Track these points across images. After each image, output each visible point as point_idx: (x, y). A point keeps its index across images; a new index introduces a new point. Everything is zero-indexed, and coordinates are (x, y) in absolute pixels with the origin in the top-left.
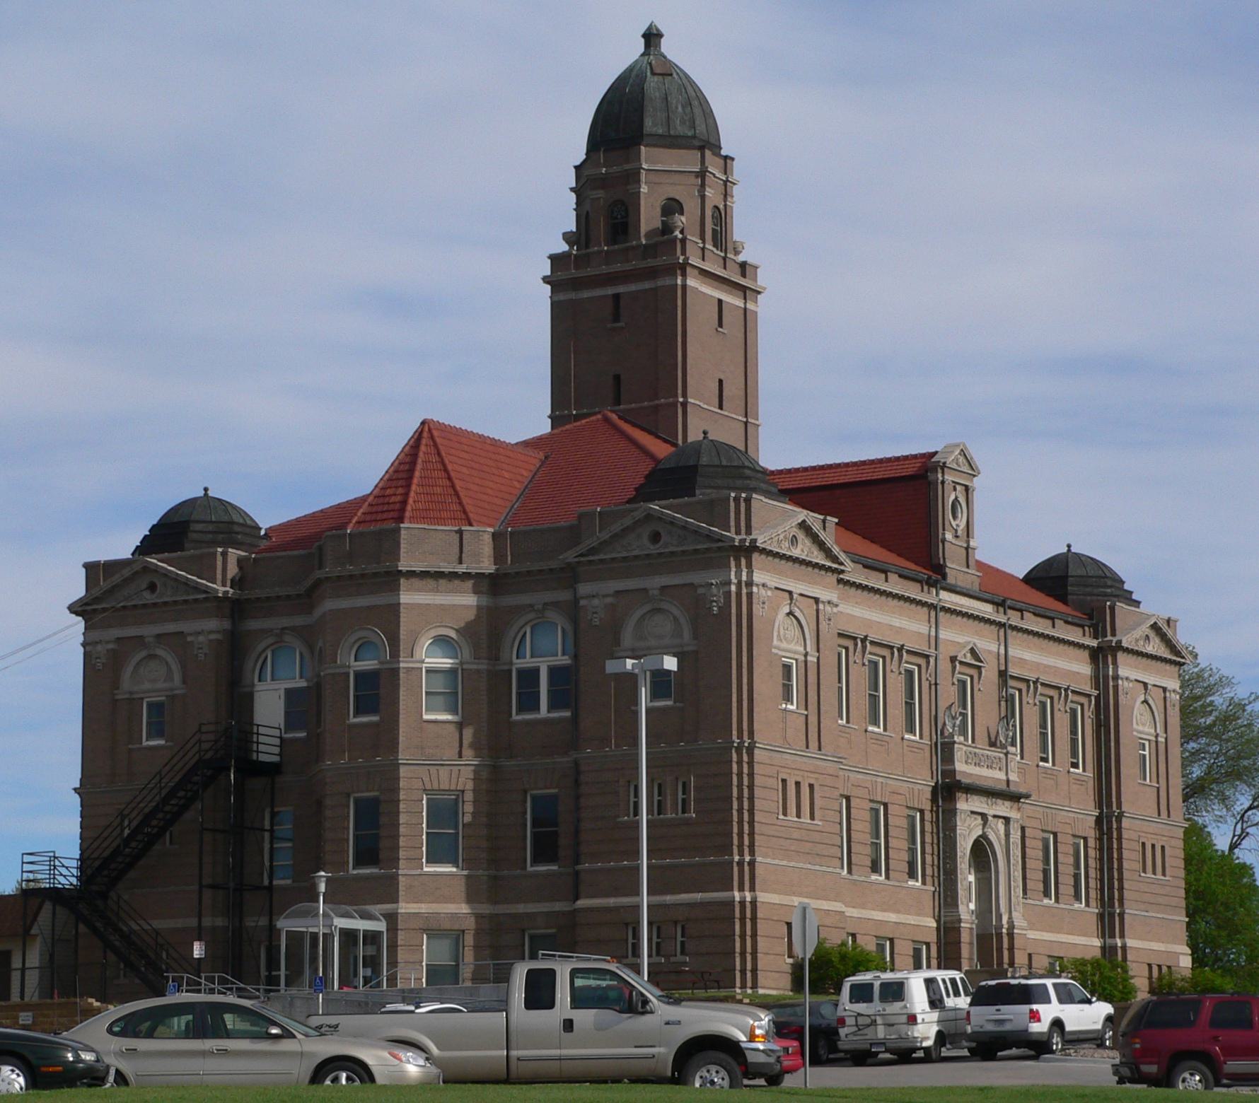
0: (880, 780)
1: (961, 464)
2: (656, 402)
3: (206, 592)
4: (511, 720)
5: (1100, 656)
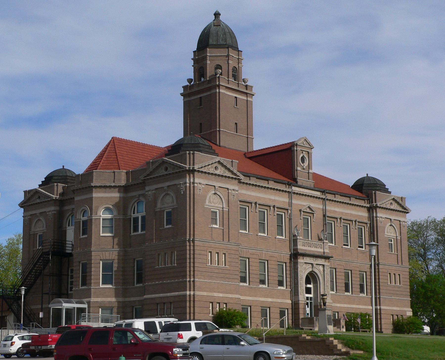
0: (264, 252)
1: (305, 144)
2: (211, 131)
4: (131, 235)
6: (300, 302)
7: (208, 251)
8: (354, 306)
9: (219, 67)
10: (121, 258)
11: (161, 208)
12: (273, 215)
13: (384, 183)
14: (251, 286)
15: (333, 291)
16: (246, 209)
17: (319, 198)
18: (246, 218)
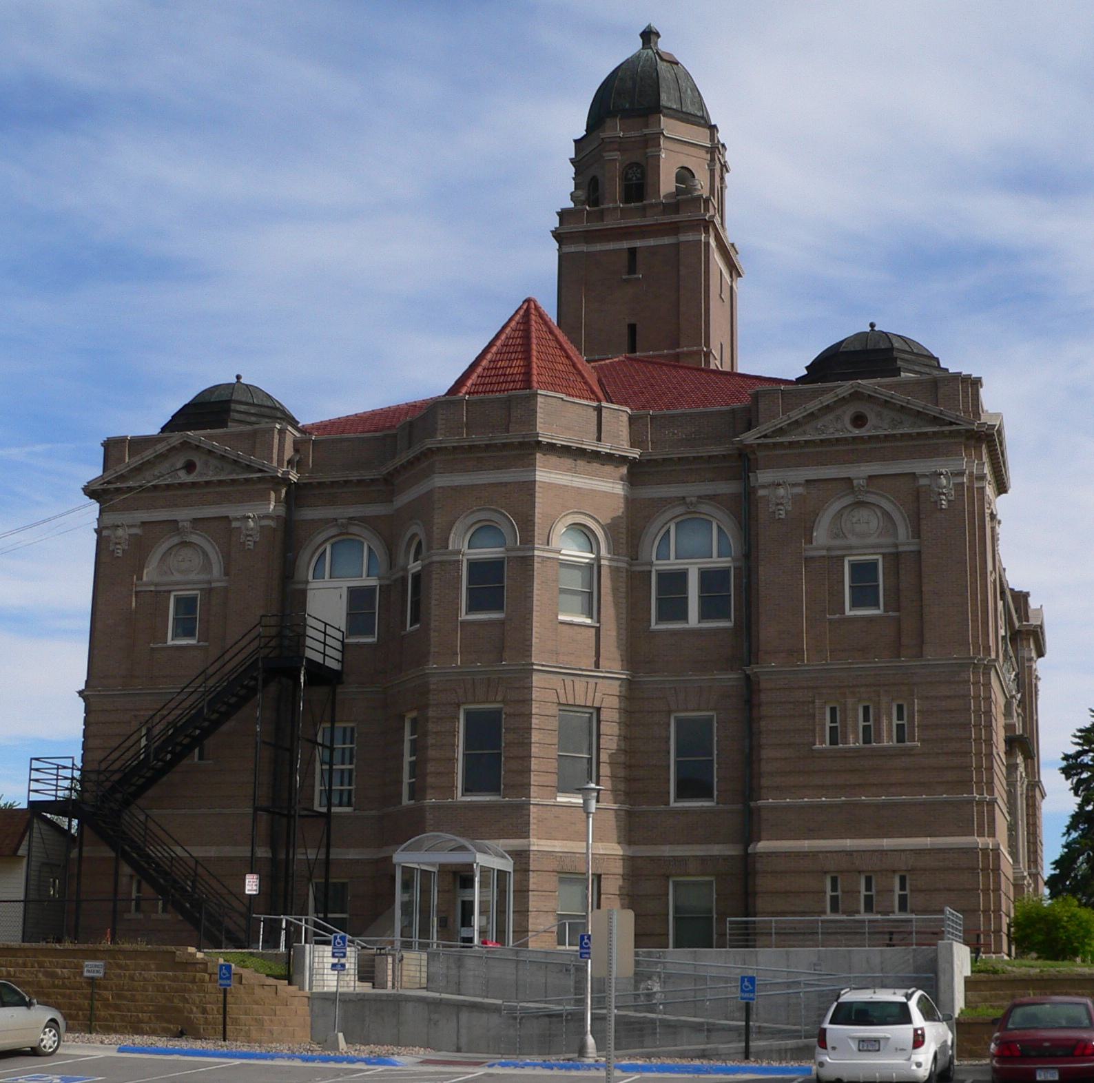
2: (678, 350)
3: (261, 471)
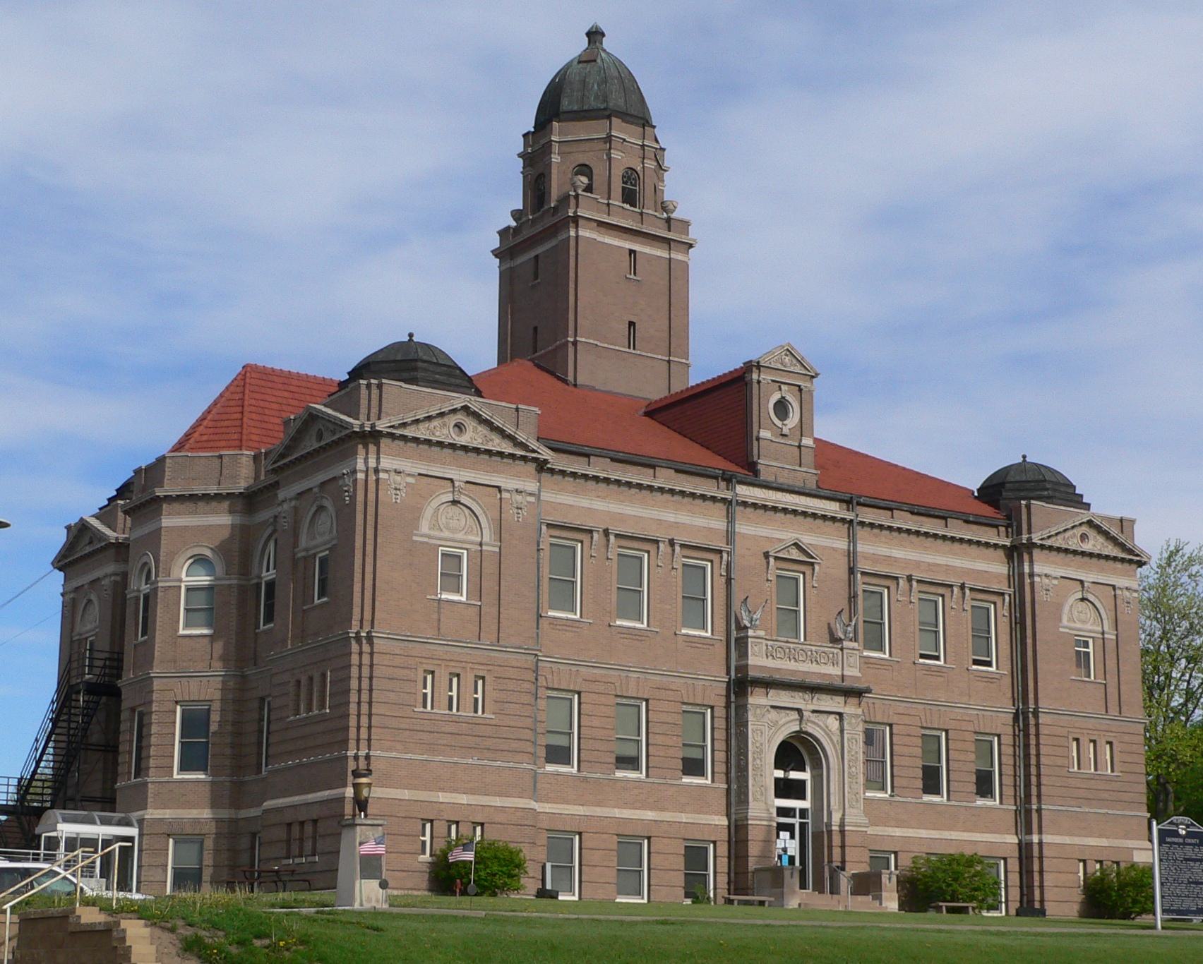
0: (631, 675)
5: (1015, 554)
6: (750, 822)
7: (1071, 738)
8: (954, 835)
9: (584, 169)
10: (230, 696)
11: (307, 550)
12: (670, 567)
13: (1069, 478)
14: (584, 774)
15: (883, 790)
16: (988, 609)
17: (834, 519)
18: (797, 606)
